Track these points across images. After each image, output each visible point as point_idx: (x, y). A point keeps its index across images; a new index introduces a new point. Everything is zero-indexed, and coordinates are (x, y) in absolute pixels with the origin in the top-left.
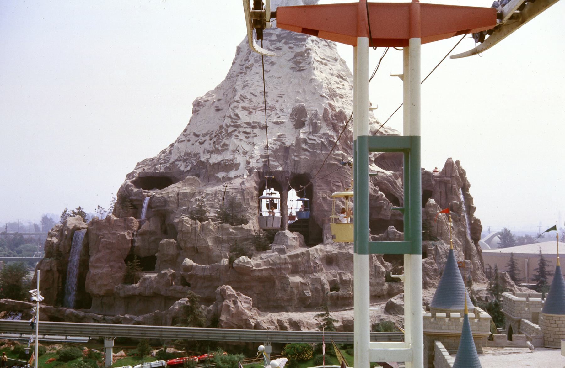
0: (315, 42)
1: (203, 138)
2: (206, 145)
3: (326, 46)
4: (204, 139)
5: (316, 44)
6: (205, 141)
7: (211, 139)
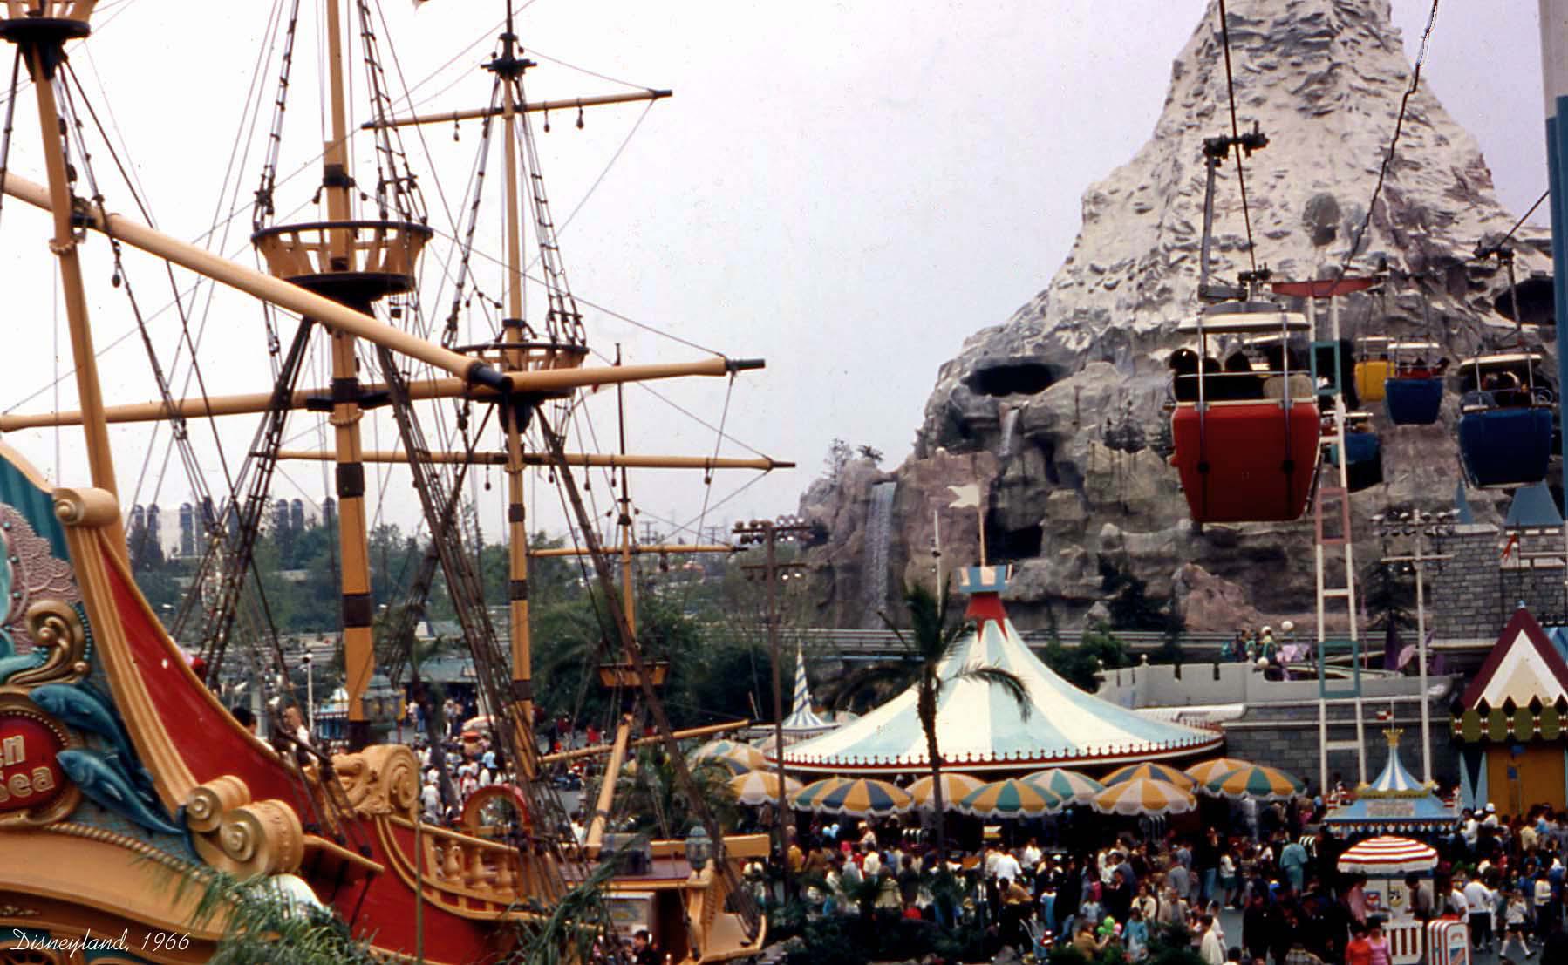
0: (1350, 44)
1: (1112, 276)
2: (1121, 291)
3: (1378, 47)
4: (1115, 278)
5: (1353, 48)
6: (1117, 283)
7: (1131, 279)
